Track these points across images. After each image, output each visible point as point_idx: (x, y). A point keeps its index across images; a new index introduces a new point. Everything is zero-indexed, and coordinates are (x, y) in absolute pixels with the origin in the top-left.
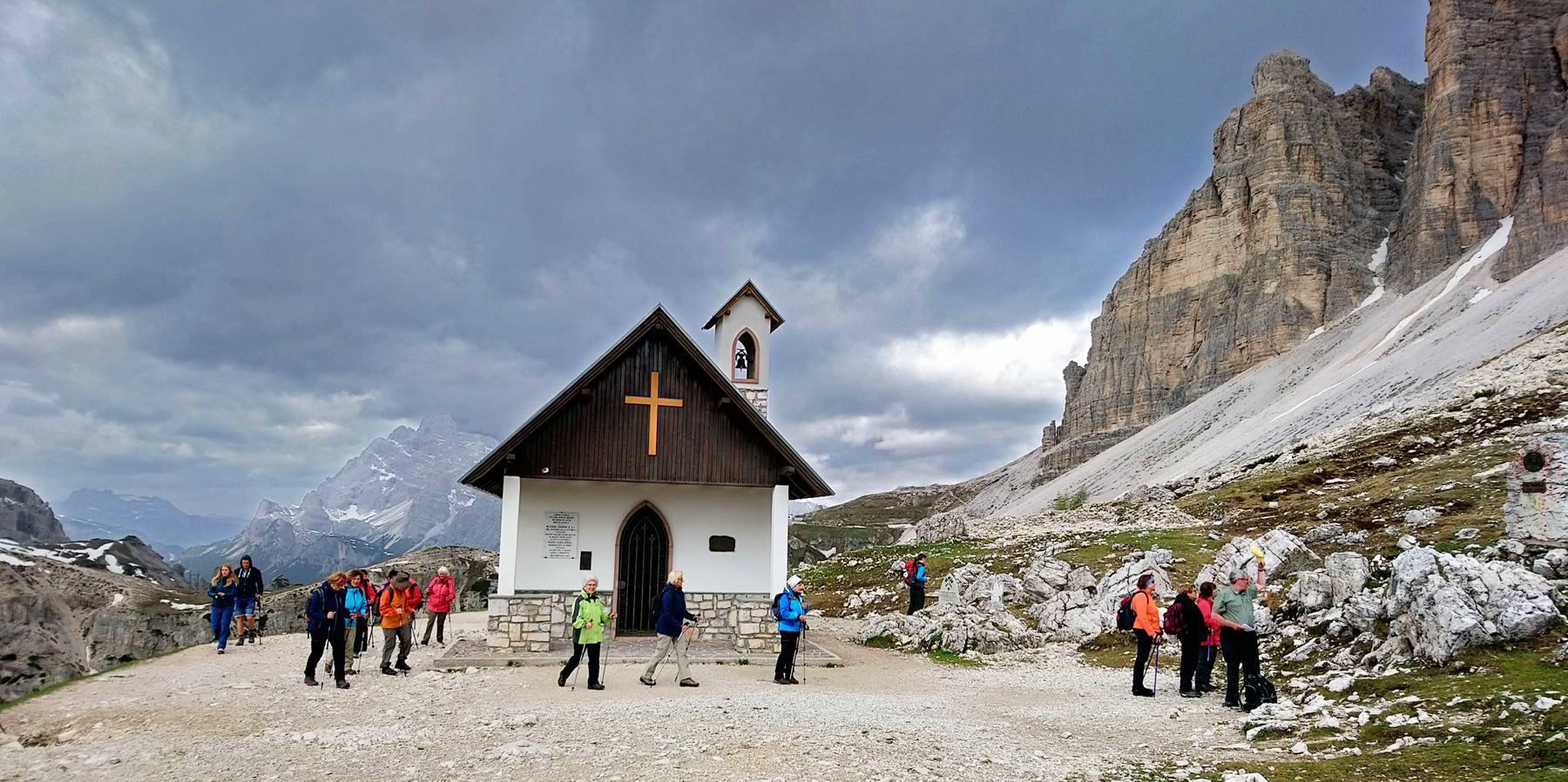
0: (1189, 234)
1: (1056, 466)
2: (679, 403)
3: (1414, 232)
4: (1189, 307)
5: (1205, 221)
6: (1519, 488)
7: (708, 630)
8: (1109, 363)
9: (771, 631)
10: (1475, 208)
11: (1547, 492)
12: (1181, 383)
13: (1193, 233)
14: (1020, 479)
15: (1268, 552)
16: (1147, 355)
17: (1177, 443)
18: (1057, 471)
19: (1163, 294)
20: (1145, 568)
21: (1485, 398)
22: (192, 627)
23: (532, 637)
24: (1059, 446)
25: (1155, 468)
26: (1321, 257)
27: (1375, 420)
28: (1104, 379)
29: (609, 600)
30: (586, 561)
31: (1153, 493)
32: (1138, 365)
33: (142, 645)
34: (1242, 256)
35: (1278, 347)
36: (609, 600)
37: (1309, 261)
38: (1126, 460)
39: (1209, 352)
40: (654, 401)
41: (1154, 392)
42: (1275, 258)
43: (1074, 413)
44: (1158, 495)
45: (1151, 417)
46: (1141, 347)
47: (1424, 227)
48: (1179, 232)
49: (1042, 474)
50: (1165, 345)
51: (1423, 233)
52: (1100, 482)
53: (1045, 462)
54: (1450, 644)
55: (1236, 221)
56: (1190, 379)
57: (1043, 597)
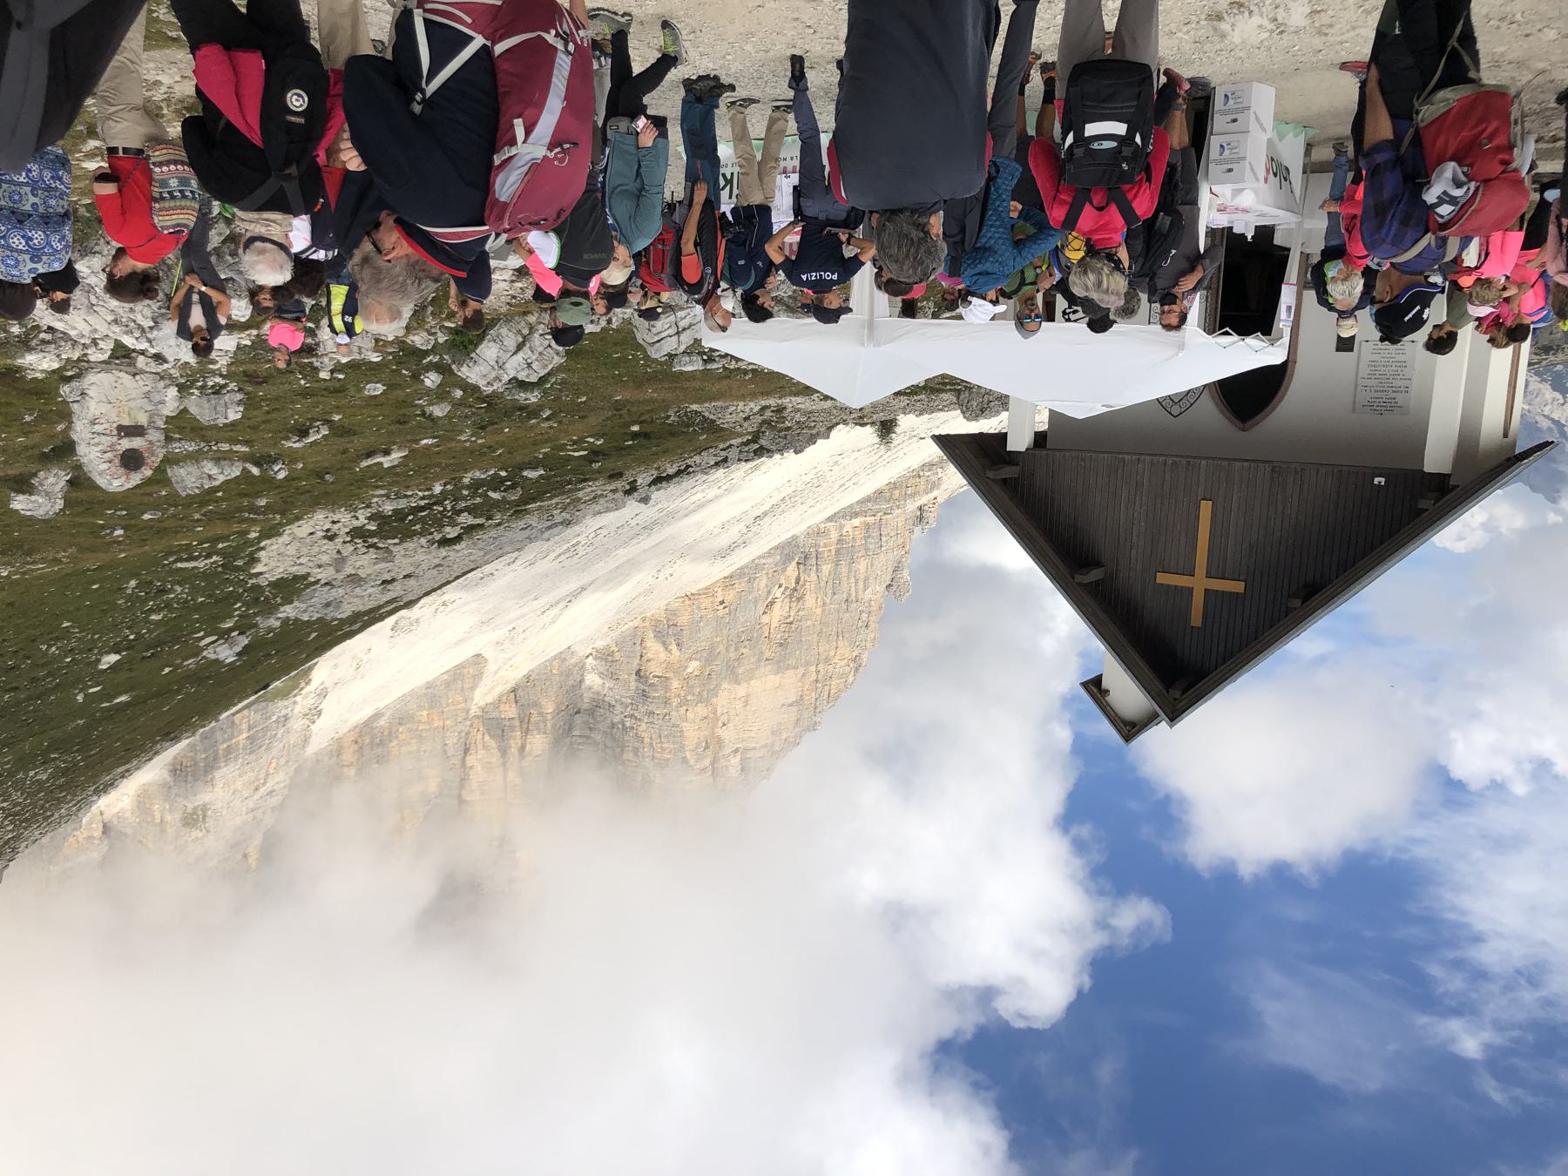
0: (773, 733)
1: (923, 479)
2: (1162, 578)
3: (558, 711)
5: (758, 745)
6: (149, 431)
10: (503, 731)
11: (115, 425)
12: (784, 570)
15: (493, 363)
18: (921, 474)
19: (801, 670)
20: (658, 344)
21: (448, 536)
24: (919, 503)
25: (812, 475)
26: (644, 695)
27: (558, 519)
28: (866, 579)
31: (782, 444)
34: (721, 701)
35: (687, 602)
37: (656, 691)
38: (844, 485)
39: (756, 602)
40: (1199, 583)
42: (689, 698)
44: (777, 441)
45: (818, 533)
46: (827, 612)
47: (549, 717)
48: (784, 736)
51: (550, 711)
54: (102, 240)
55: (726, 741)
57: (788, 306)
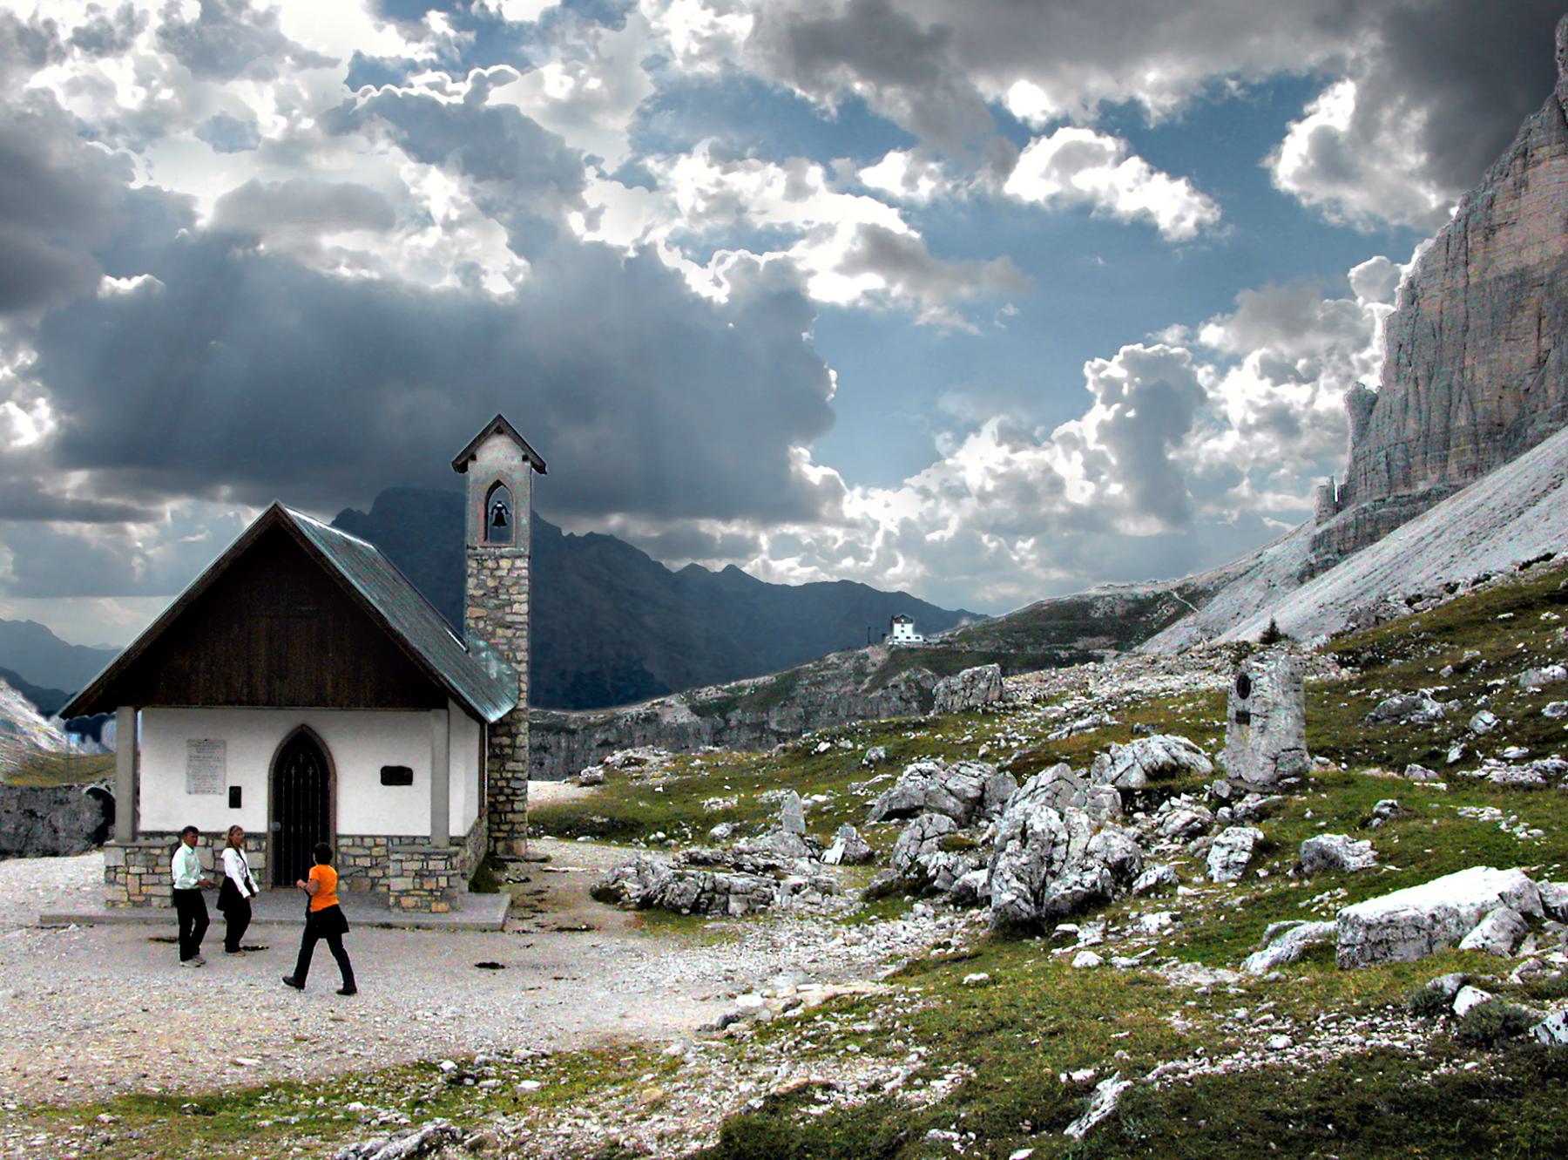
4: (1529, 297)
5: (1548, 163)
7: (381, 882)
8: (1411, 387)
9: (427, 887)
13: (1531, 183)
14: (1282, 570)
16: (1468, 374)
17: (1512, 510)
18: (1337, 556)
22: (74, 806)
23: (152, 890)
24: (1340, 515)
25: (1480, 548)
29: (264, 844)
30: (235, 798)
31: (1381, 609)
32: (1456, 389)
33: (12, 831)
36: (264, 844)
41: (1482, 430)
43: (1361, 464)
45: (1477, 470)
48: (1510, 181)
49: (1314, 562)
50: (1493, 356)
52: (1397, 574)
53: (1317, 542)
56: (1533, 408)
